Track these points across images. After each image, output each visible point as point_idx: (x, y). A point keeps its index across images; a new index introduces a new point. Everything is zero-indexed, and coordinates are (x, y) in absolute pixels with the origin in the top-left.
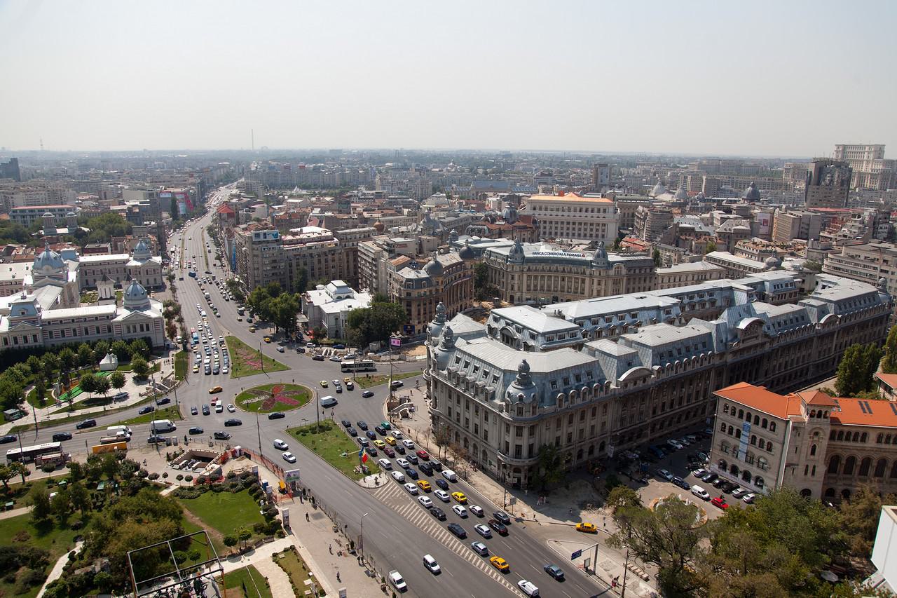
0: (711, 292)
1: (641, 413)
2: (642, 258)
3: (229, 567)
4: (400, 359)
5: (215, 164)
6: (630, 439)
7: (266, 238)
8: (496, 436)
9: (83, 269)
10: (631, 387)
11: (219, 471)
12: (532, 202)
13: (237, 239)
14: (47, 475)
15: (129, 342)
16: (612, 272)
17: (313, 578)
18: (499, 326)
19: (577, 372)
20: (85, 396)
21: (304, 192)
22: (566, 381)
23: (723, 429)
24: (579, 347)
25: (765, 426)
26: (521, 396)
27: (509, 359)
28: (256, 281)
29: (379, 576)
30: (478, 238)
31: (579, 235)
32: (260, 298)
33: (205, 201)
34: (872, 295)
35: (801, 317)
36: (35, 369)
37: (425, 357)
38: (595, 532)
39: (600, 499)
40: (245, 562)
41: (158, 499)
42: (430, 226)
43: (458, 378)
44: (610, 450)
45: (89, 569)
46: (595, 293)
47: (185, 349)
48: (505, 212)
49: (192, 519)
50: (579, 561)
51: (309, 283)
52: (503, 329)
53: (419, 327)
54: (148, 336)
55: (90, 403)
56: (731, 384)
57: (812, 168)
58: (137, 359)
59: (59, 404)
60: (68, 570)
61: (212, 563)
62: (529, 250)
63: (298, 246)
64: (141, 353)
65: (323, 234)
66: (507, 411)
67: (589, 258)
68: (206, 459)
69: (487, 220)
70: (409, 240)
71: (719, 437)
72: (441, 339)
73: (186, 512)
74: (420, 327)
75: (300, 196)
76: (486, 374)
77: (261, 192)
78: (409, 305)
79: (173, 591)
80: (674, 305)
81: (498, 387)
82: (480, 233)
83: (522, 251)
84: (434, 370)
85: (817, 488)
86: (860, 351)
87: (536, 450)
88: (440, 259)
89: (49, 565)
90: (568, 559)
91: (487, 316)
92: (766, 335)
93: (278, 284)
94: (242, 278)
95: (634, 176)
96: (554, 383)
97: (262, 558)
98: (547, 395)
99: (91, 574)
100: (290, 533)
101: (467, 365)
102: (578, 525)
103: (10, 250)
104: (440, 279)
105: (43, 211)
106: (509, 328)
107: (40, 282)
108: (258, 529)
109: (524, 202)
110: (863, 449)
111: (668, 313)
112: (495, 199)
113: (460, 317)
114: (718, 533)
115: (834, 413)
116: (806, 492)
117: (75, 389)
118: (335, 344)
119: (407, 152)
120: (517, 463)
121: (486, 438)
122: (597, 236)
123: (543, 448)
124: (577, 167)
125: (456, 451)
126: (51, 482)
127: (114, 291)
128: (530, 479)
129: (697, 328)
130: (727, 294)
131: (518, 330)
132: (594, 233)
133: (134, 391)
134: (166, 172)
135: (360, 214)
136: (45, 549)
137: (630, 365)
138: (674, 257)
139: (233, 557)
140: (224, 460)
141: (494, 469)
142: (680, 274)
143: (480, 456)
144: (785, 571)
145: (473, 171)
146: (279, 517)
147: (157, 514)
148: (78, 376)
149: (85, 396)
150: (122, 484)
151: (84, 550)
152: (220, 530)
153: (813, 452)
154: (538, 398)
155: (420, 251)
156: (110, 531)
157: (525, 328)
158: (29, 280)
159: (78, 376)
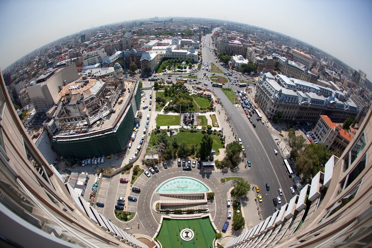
0: (328, 91)
1: (304, 113)
2: (316, 75)
3: (200, 114)
4: (252, 79)
5: (216, 22)
6: (299, 118)
8: (269, 105)
9: (182, 42)
10: (303, 106)
11: (203, 93)
12: (293, 51)
13: (218, 40)
14: (168, 85)
15: (189, 59)
16: (308, 76)
17: (217, 123)
18: (278, 78)
19: (293, 97)
20: (178, 69)
21: (236, 32)
22: (289, 98)
23: (318, 125)
24: (295, 91)
25: (327, 128)
26: (278, 98)
27: (278, 87)
28: (221, 51)
29: (232, 128)
30: (278, 55)
31: (303, 63)
32: (221, 55)
33: (212, 30)
34: (355, 108)
35: (342, 106)
36: (169, 62)
37: (258, 80)
38: (283, 136)
39: (287, 129)
40: (204, 114)
41: (188, 95)
42: (267, 48)
43: (264, 88)
44: (294, 119)
45: (173, 106)
46: (303, 79)
47: (201, 63)
48: (286, 51)
49: (195, 102)
50: (277, 141)
51: (234, 54)
52: (279, 79)
53: (259, 72)
55: (179, 71)
56: (324, 115)
57: (354, 72)
58: (190, 63)
59: (173, 70)
60: (169, 105)
61: (197, 112)
62: (290, 62)
63: (232, 45)
64: (191, 62)
65: (239, 43)
66: (273, 100)
67: (304, 70)
68: (201, 89)
69: (281, 51)
70: (260, 50)
71: (317, 126)
72: (263, 77)
73: (194, 100)
74: (259, 72)
75: (235, 33)
76: (271, 89)
77: (226, 30)
78: (257, 66)
79: (188, 116)
80: (319, 90)
81: (273, 93)
82: (279, 54)
83: (288, 62)
84: (259, 84)
85: (329, 146)
86: (350, 120)
87: (277, 112)
88: (267, 57)
89: (166, 103)
90: (274, 140)
91: (276, 75)
92: (335, 107)
93: (226, 52)
94: (217, 49)
95: (318, 54)
96: (286, 97)
97: (208, 115)
98: (284, 100)
99: (173, 107)
100: (215, 111)
101: (267, 85)
102: (280, 133)
103: (168, 37)
104: (266, 62)
105: (176, 29)
106: (280, 80)
107: (173, 44)
108: (208, 108)
109: (291, 50)
110: (340, 142)
111: (317, 91)
112: (284, 47)
113: (269, 73)
114: (308, 147)
115: (340, 131)
116: (327, 146)
117: (176, 68)
118: (237, 70)
119: (264, 29)
120: (271, 113)
121: (267, 105)
122: (307, 65)
123: (279, 112)
124: (306, 47)
125: (259, 105)
126: (168, 86)
127: (188, 47)
128: (273, 118)
129: (322, 98)
130: (331, 93)
131: (282, 81)
132: (306, 64)
133: (188, 70)
134: (204, 23)
135: (249, 41)
136: (165, 99)
137: (305, 100)
138: (322, 78)
139: (201, 112)
140: (204, 91)
141: (266, 113)
142: (322, 83)
143: (264, 109)
144: (315, 161)
145: (280, 38)
146: (214, 107)
147: (188, 99)
148: (177, 65)
149: (178, 69)
150: (182, 90)
151: (172, 102)
152: (200, 106)
153: (332, 138)
154: (282, 100)
155: (263, 54)
156: (178, 99)
157: (284, 81)
158: (171, 43)
159: (177, 65)
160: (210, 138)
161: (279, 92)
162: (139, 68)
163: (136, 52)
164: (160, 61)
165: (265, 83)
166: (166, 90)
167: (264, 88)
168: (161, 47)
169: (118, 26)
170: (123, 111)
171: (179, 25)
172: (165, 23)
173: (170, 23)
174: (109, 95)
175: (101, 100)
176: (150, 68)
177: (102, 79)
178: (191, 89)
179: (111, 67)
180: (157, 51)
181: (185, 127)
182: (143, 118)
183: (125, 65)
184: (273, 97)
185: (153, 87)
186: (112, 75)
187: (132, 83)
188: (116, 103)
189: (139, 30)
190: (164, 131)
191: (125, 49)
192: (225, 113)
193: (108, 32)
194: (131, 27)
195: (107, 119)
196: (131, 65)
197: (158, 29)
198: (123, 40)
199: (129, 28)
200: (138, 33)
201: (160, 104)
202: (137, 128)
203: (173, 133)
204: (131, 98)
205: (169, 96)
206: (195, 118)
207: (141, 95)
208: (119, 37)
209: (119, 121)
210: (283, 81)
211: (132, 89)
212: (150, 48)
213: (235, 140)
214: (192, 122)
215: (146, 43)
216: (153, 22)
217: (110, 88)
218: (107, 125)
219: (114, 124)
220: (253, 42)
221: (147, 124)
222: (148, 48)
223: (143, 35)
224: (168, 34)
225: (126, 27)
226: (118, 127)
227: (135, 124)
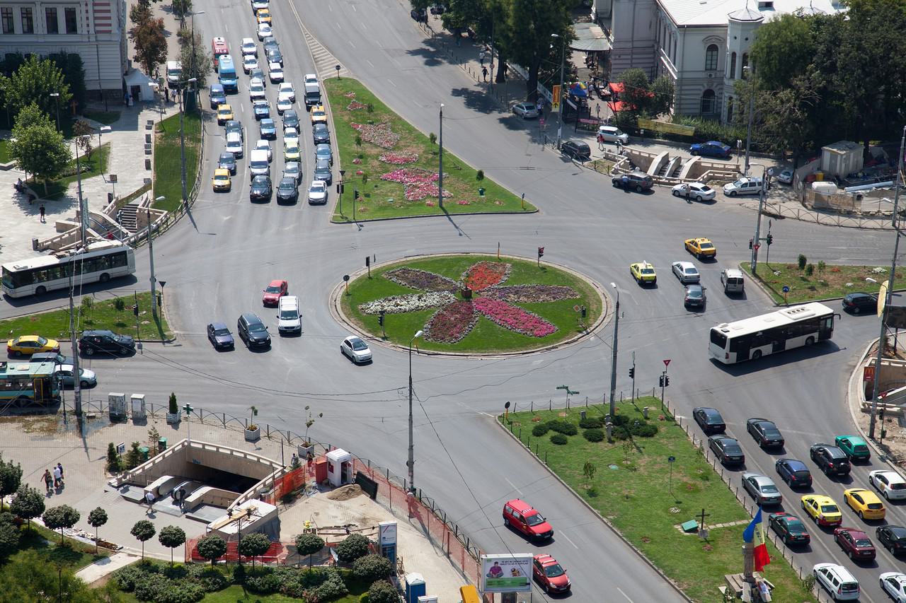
11: (271, 526)
47: (192, 110)
54: (70, 50)
64: (49, 107)
118: (699, 137)
140: (290, 492)
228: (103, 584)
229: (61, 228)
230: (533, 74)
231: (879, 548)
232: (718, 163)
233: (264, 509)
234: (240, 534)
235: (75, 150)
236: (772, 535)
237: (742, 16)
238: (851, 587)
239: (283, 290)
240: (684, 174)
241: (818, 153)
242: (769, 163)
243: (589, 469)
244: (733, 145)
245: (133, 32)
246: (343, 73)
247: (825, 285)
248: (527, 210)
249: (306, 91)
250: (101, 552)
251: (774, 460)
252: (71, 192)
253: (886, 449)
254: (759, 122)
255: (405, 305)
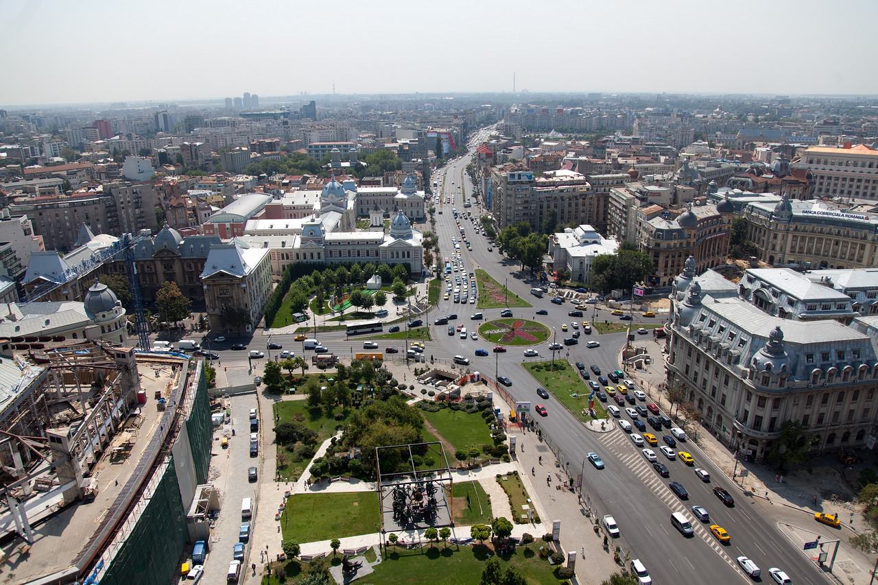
3: (458, 478)
4: (641, 310)
7: (520, 178)
9: (360, 198)
11: (458, 392)
13: (493, 179)
15: (392, 266)
17: (531, 504)
20: (353, 309)
21: (560, 135)
24: (847, 321)
27: (760, 324)
28: (507, 220)
29: (594, 517)
32: (511, 236)
33: (466, 141)
36: (317, 282)
37: (668, 310)
38: (838, 527)
39: (849, 491)
40: (471, 477)
41: (404, 407)
42: (688, 175)
45: (345, 454)
47: (439, 277)
48: (774, 164)
49: (431, 431)
50: (814, 553)
51: (558, 226)
52: (758, 291)
53: (664, 279)
54: (408, 262)
59: (333, 314)
60: (330, 451)
62: (799, 208)
63: (551, 189)
64: (402, 277)
65: (576, 178)
66: (751, 378)
70: (663, 189)
73: (426, 422)
75: (556, 140)
76: (732, 336)
77: (519, 134)
78: (657, 255)
79: (409, 488)
81: (744, 352)
82: (743, 186)
83: (790, 208)
84: (676, 325)
87: (778, 424)
88: (695, 210)
89: (316, 444)
90: (801, 548)
91: (741, 276)
93: (528, 224)
96: (810, 356)
97: (487, 476)
99: (347, 459)
100: (515, 459)
101: (712, 324)
102: (818, 515)
103: (306, 179)
104: (693, 232)
105: (331, 146)
106: (765, 290)
108: (487, 450)
109: (798, 154)
112: (764, 149)
113: (710, 273)
117: (346, 302)
118: (578, 287)
120: (753, 434)
121: (723, 402)
123: (787, 424)
126: (322, 377)
127: (383, 219)
128: (767, 453)
131: (775, 294)
133: (392, 310)
135: (615, 160)
139: (462, 470)
140: (463, 383)
141: (728, 436)
143: (714, 420)
145: (742, 118)
146: (507, 443)
147: (402, 420)
148: (349, 291)
149: (353, 309)
150: (376, 389)
151: (343, 438)
152: (454, 444)
154: (788, 369)
155: (675, 201)
156: (364, 426)
157: (783, 292)
158: (317, 206)
159: (349, 291)
160: (511, 575)
161: (771, 339)
162: (199, 306)
163: (182, 242)
164: (280, 278)
165: (699, 317)
166: (314, 392)
167: (701, 337)
168: (279, 224)
169: (89, 122)
170: (132, 491)
171: (342, 130)
172: (285, 123)
173: (308, 122)
174: (63, 423)
175: (21, 448)
176: (242, 307)
177: (26, 352)
178: (411, 380)
179: (67, 299)
180: (266, 239)
181: (403, 536)
182: (222, 514)
183: (137, 298)
184: (748, 366)
185: (259, 385)
186: (75, 336)
187: (173, 369)
188: (98, 455)
189: (183, 150)
190: (319, 566)
191: (130, 227)
192: (553, 460)
193: (41, 145)
194: (149, 132)
195: (46, 533)
196: (161, 295)
197: (260, 147)
198: (116, 187)
199: (141, 136)
200: (180, 160)
201: (291, 450)
202: (195, 563)
203: (358, 566)
204: (171, 434)
205: (329, 418)
206: (439, 496)
207: (214, 419)
208: (99, 173)
209: (112, 535)
210: (778, 293)
211: (172, 398)
212: (238, 228)
213: (617, 570)
214: (428, 514)
215: (222, 205)
216: (241, 115)
217: (68, 390)
218: (44, 566)
219: (89, 555)
220: (631, 161)
221: (244, 540)
222: (228, 225)
223: (205, 169)
224: (304, 168)
225: (124, 131)
226: (107, 565)
227: (187, 552)
228: (413, 405)
229: (404, 309)
230: (532, 269)
231: (625, 401)
232: (583, 294)
233: (456, 387)
234: (449, 394)
235: (408, 288)
236: (597, 398)
237: (589, 254)
238: (618, 412)
239: (462, 326)
240: (574, 297)
241: (610, 292)
242: (597, 295)
243: (546, 379)
244: (587, 289)
245: (424, 257)
246: (480, 268)
247: (612, 328)
248: (530, 306)
249: (496, 376)
250: (413, 397)
251: (598, 377)
252: (407, 300)
253: (628, 374)
254: (594, 283)
255: (496, 332)
